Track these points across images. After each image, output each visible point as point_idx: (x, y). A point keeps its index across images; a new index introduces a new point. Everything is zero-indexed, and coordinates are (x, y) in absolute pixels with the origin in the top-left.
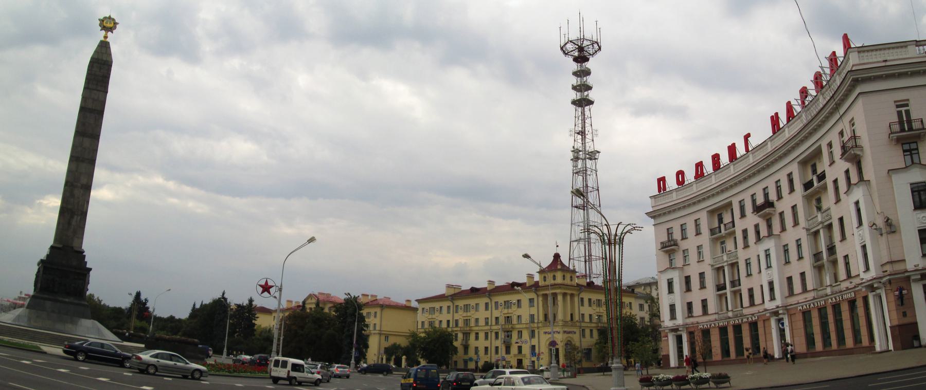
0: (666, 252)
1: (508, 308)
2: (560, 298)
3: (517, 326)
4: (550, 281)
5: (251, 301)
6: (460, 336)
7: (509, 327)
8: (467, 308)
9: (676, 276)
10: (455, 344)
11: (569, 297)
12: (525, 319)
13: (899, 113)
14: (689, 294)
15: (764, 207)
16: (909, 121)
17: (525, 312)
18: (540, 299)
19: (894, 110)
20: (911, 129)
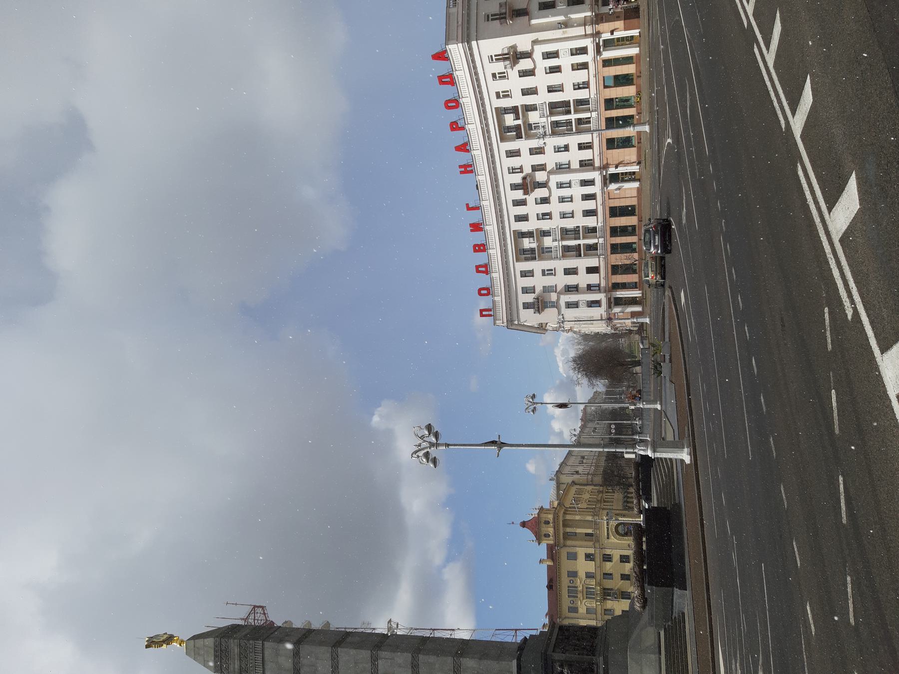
0: (543, 310)
1: (576, 592)
2: (568, 530)
3: (598, 578)
4: (551, 531)
5: (328, 624)
6: (610, 604)
7: (598, 558)
8: (573, 592)
9: (565, 298)
10: (618, 612)
11: (568, 530)
12: (591, 567)
13: (492, 20)
14: (578, 184)
15: (527, 185)
16: (501, 14)
17: (583, 567)
18: (569, 543)
19: (490, 22)
20: (505, 13)
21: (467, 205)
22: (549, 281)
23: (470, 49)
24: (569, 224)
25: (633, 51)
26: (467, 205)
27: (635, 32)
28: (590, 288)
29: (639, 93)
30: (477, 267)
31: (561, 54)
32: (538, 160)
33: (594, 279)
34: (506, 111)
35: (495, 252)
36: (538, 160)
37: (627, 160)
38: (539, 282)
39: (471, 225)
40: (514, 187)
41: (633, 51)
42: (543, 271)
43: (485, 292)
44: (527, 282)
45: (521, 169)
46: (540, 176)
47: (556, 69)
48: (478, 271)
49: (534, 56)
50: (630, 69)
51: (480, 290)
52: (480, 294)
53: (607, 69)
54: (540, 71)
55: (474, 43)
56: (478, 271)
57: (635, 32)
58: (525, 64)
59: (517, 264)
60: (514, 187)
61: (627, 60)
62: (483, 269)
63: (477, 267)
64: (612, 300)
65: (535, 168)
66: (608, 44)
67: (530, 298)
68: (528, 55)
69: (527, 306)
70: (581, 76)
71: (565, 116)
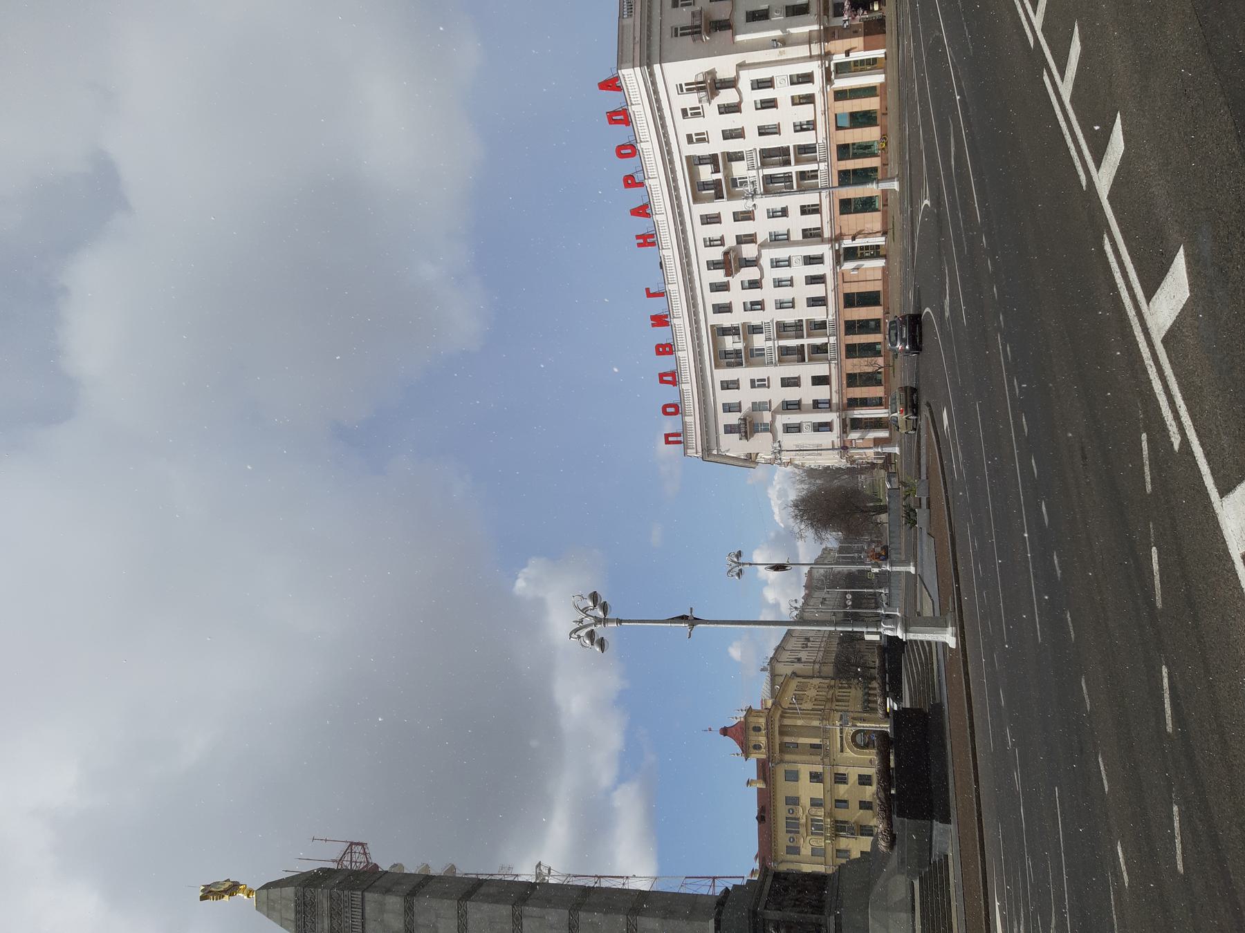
19: (680, 39)
21: (647, 290)
22: (761, 395)
23: (652, 74)
24: (789, 316)
25: (876, 79)
26: (647, 290)
27: (879, 53)
28: (816, 405)
29: (884, 137)
30: (661, 375)
31: (776, 83)
32: (745, 228)
33: (822, 392)
34: (701, 160)
35: (685, 354)
36: (745, 228)
37: (868, 229)
38: (746, 397)
39: (653, 318)
40: (713, 265)
41: (876, 79)
42: (753, 381)
43: (672, 409)
44: (730, 396)
45: (722, 241)
46: (749, 251)
47: (770, 104)
48: (662, 381)
49: (740, 85)
50: (871, 104)
51: (665, 407)
52: (665, 413)
53: (840, 103)
54: (747, 106)
55: (657, 67)
56: (662, 381)
57: (879, 53)
58: (727, 96)
59: (716, 372)
60: (713, 265)
61: (869, 91)
62: (670, 378)
63: (661, 375)
64: (848, 421)
65: (741, 240)
66: (843, 69)
67: (733, 418)
68: (731, 83)
69: (729, 429)
70: (804, 113)
71: (782, 167)
